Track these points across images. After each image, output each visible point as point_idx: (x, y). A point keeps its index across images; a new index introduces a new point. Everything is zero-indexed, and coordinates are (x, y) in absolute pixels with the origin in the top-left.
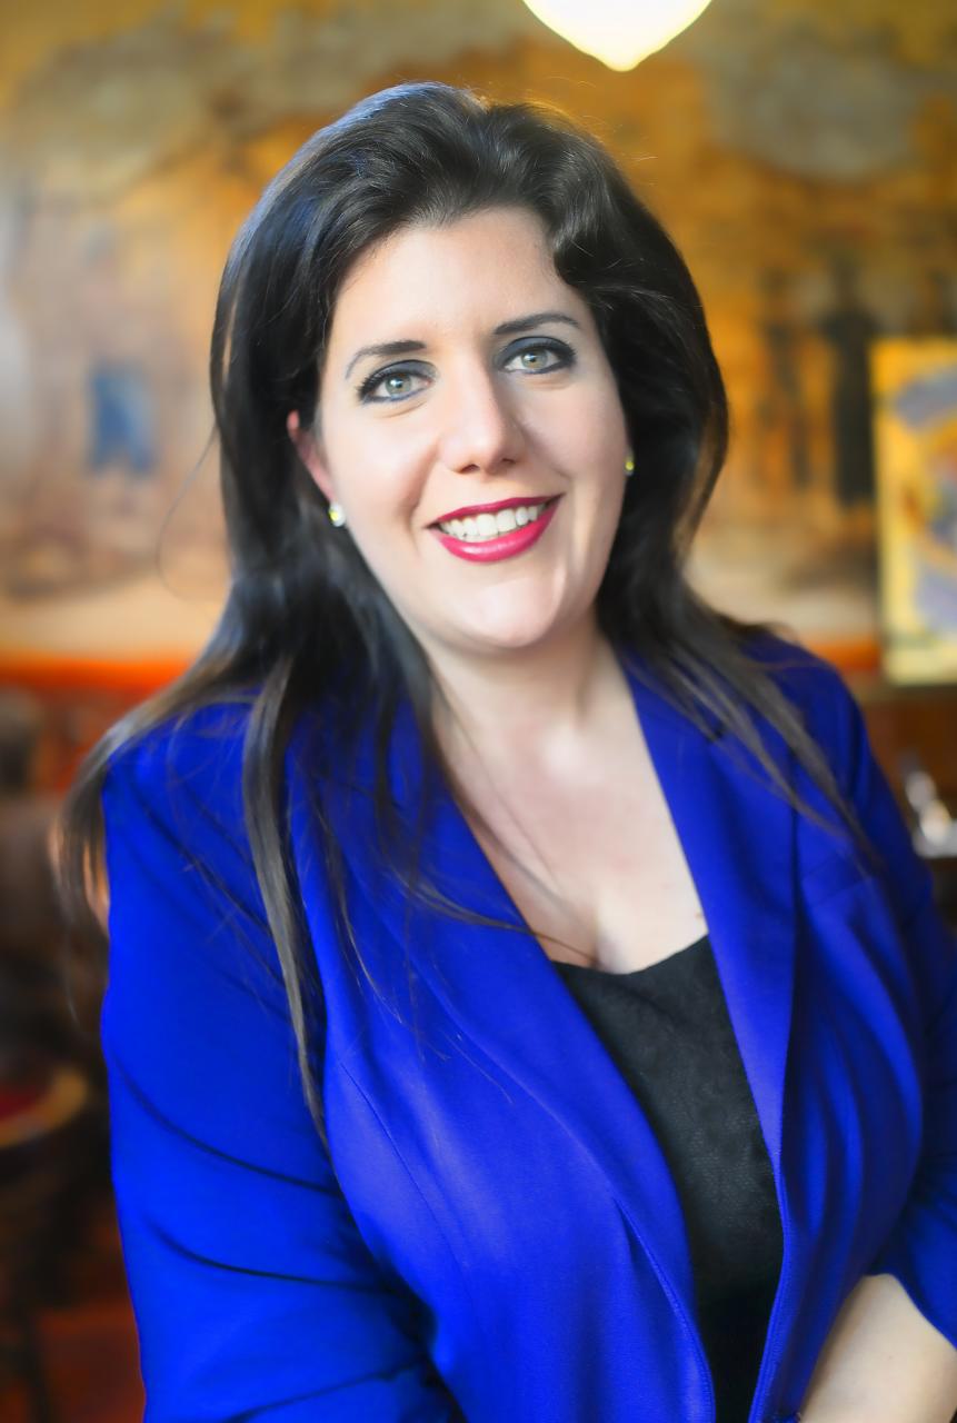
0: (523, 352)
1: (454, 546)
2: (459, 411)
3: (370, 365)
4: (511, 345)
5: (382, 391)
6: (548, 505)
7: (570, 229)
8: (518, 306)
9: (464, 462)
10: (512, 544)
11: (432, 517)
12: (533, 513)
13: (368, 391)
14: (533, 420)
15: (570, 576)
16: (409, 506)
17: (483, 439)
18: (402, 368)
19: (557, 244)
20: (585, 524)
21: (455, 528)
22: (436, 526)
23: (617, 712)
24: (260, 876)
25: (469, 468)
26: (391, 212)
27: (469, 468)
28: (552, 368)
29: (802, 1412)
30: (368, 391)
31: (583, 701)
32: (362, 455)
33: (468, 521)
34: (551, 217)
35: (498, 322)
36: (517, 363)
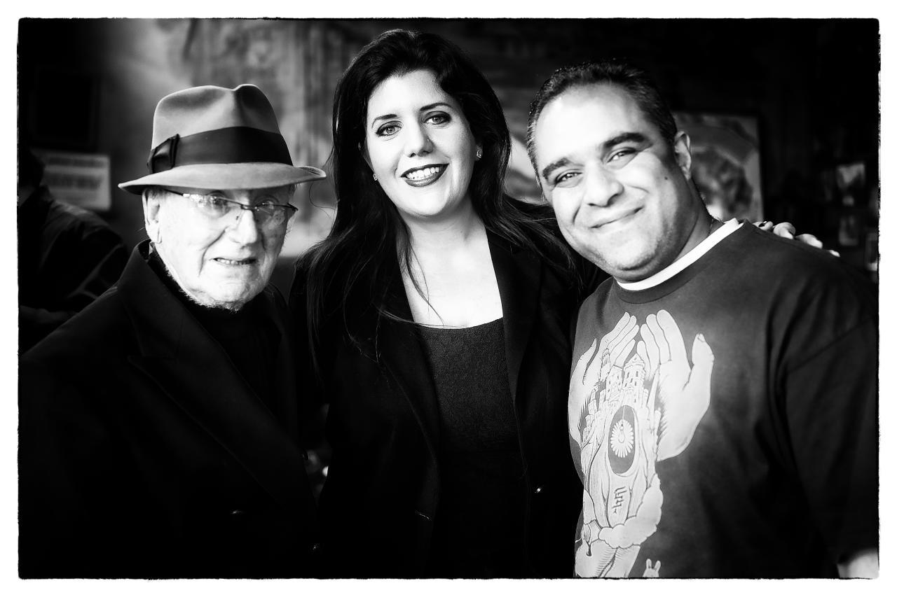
0: (432, 117)
1: (411, 184)
2: (410, 137)
3: (379, 123)
4: (425, 114)
5: (385, 132)
6: (443, 167)
7: (445, 74)
8: (428, 101)
9: (410, 153)
10: (432, 179)
11: (402, 173)
12: (437, 170)
13: (380, 132)
14: (435, 139)
15: (451, 191)
16: (395, 170)
17: (417, 144)
18: (390, 125)
19: (441, 79)
20: (456, 176)
21: (410, 176)
22: (405, 175)
23: (480, 245)
24: (429, 326)
25: (412, 155)
26: (384, 74)
27: (412, 155)
28: (442, 122)
29: (183, 165)
30: (380, 132)
31: (467, 236)
32: (383, 153)
33: (414, 173)
34: (504, 194)
35: (421, 106)
36: (431, 121)
